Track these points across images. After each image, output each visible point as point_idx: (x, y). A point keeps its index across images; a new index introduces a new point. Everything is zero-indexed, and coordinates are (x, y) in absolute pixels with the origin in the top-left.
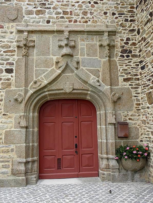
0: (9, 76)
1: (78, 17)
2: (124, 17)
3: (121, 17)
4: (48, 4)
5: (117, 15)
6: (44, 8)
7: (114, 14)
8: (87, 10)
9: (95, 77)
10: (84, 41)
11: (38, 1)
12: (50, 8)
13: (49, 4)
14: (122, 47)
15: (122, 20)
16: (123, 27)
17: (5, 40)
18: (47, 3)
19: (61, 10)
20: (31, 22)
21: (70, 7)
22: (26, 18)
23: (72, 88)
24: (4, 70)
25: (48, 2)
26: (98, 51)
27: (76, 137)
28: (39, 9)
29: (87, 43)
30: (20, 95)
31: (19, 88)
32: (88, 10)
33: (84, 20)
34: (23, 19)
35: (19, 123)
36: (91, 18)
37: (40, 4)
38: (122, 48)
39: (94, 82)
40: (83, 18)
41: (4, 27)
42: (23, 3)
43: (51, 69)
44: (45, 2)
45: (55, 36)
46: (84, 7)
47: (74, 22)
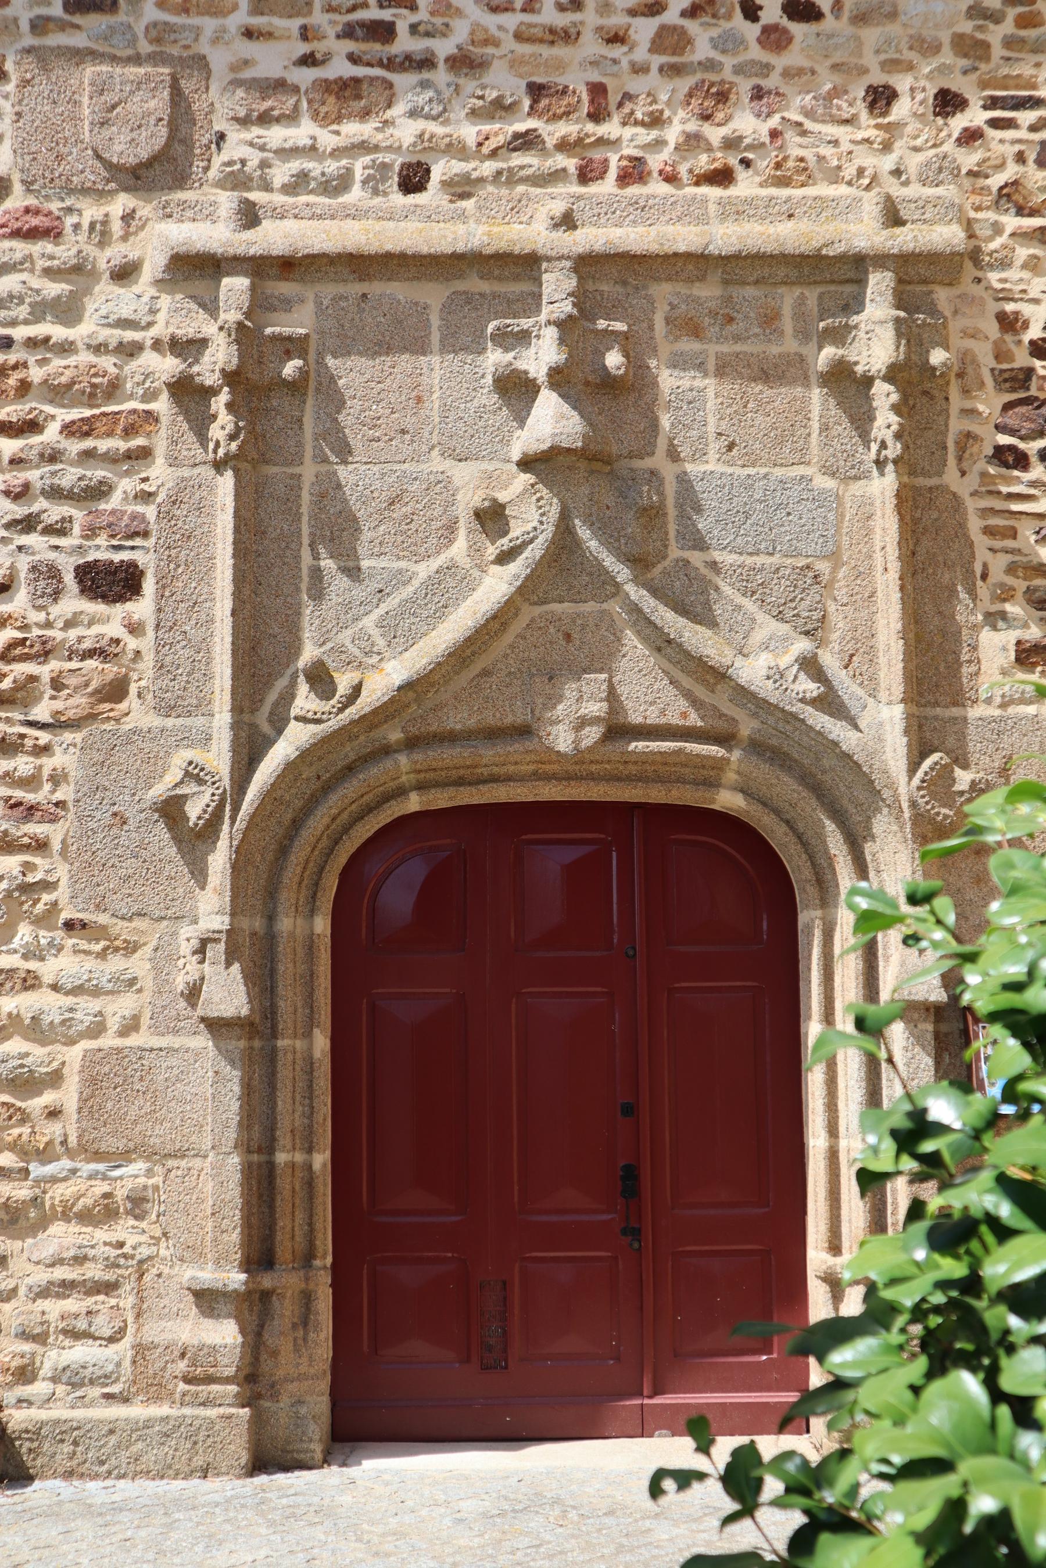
0: (110, 621)
1: (654, 134)
2: (1033, 128)
3: (1009, 124)
4: (414, 29)
5: (976, 116)
6: (380, 64)
7: (948, 102)
8: (728, 70)
9: (784, 628)
10: (696, 332)
11: (330, 9)
12: (427, 62)
13: (421, 28)
14: (1012, 379)
15: (1020, 158)
16: (1020, 211)
17: (78, 333)
18: (403, 20)
19: (521, 76)
20: (277, 183)
21: (591, 46)
22: (238, 146)
23: (595, 721)
24: (69, 578)
25: (413, 8)
26: (815, 415)
27: (628, 1110)
28: (340, 68)
29: (725, 348)
30: (194, 775)
31: (188, 721)
32: (738, 70)
33: (703, 162)
34: (217, 161)
35: (193, 993)
36: (763, 144)
37: (348, 32)
38: (1013, 390)
39: (777, 675)
40: (692, 142)
41: (68, 229)
42: (209, 24)
43: (436, 563)
44: (386, 15)
45: (468, 298)
46: (702, 50)
47: (625, 178)
